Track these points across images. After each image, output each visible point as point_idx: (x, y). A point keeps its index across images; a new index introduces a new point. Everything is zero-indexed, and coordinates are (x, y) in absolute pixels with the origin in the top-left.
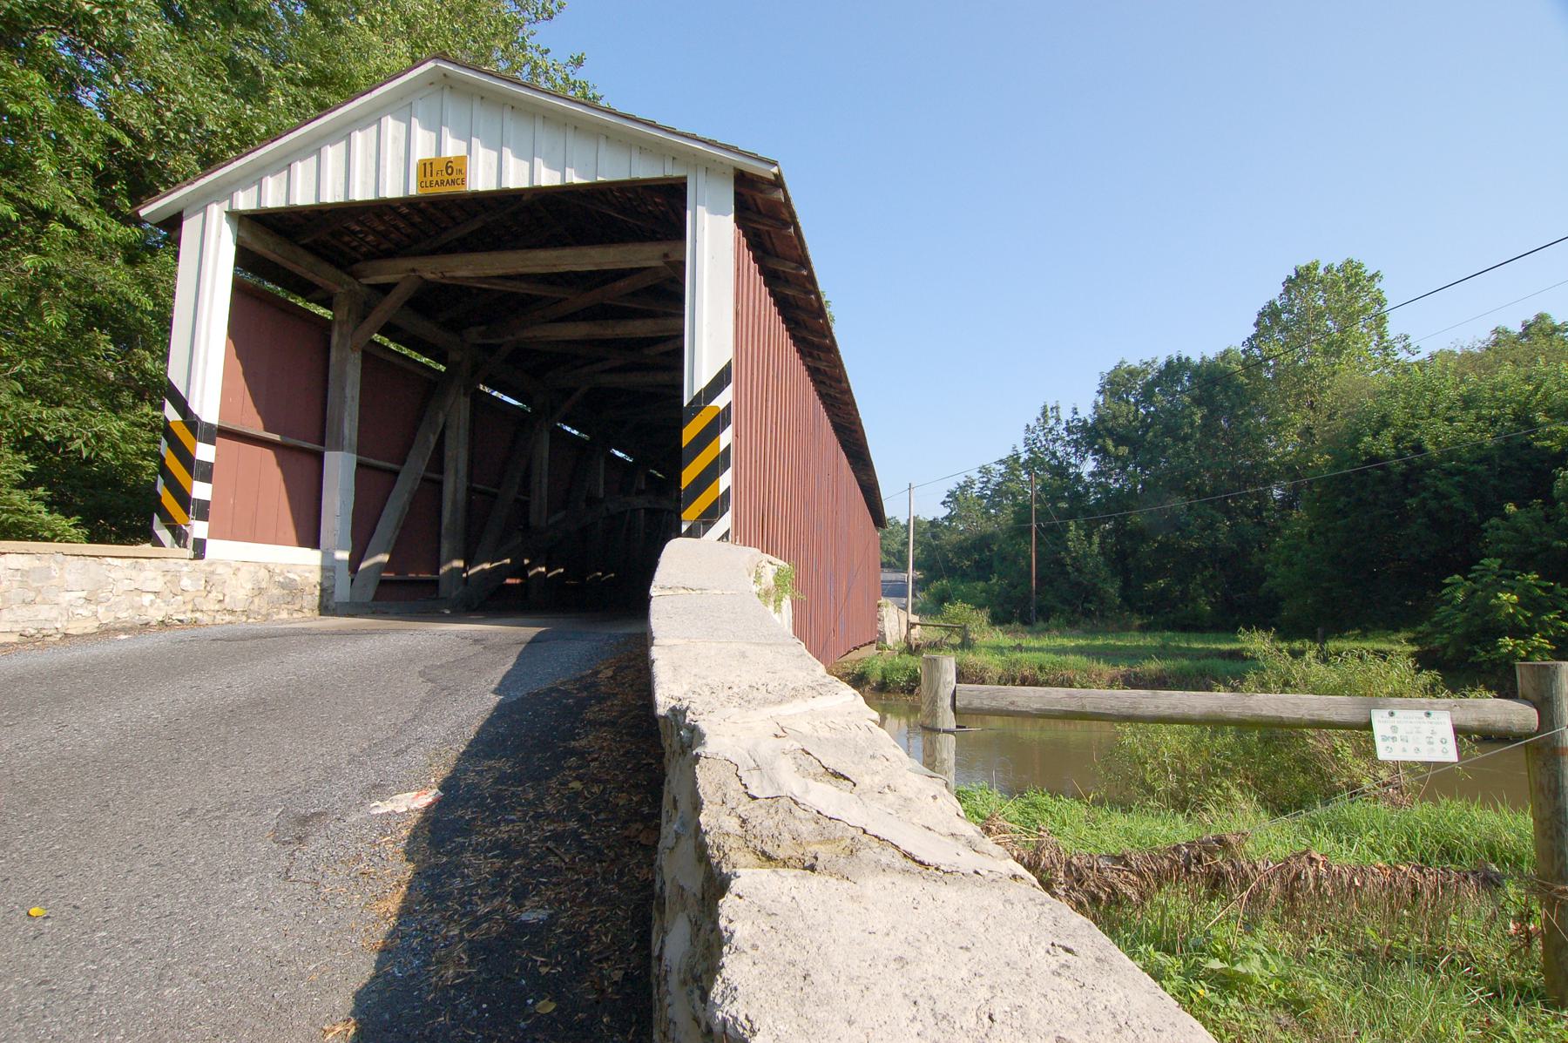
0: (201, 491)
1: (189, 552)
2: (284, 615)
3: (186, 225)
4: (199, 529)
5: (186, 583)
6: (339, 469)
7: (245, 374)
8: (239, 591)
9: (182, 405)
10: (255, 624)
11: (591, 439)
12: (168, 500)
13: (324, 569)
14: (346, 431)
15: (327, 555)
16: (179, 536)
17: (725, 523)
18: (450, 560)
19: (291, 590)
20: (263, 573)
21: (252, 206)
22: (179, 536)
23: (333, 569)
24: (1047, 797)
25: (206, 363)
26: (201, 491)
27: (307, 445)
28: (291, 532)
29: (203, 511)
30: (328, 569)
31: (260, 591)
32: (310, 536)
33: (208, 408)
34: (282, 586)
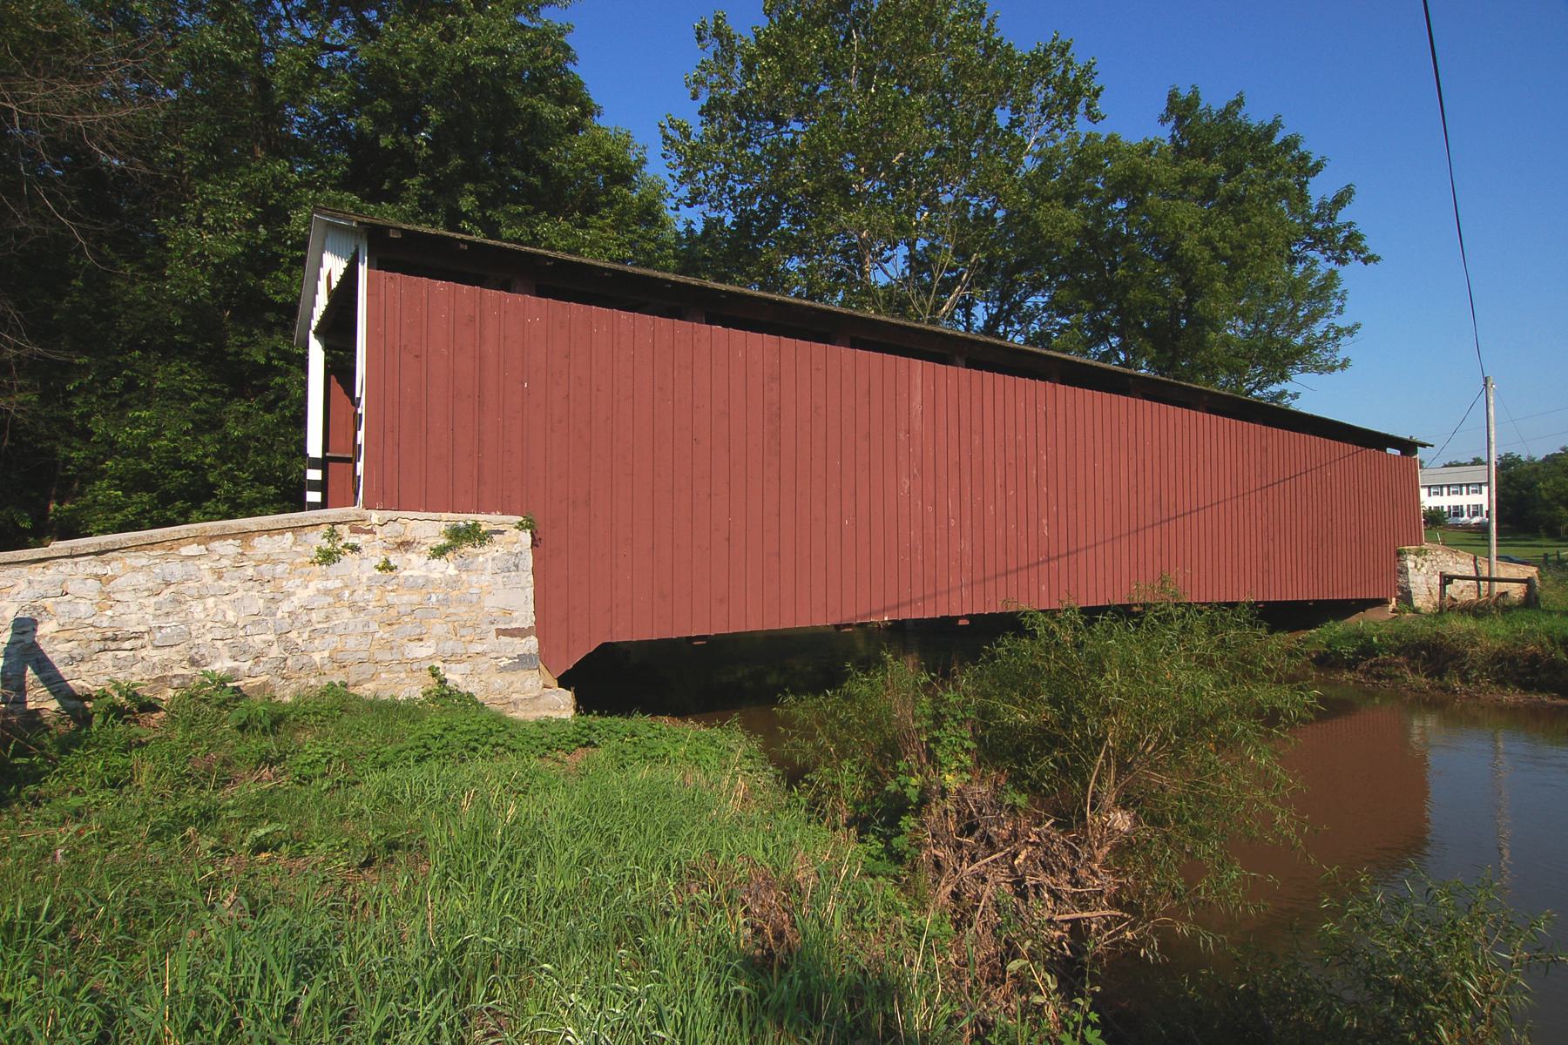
28: (376, 266)
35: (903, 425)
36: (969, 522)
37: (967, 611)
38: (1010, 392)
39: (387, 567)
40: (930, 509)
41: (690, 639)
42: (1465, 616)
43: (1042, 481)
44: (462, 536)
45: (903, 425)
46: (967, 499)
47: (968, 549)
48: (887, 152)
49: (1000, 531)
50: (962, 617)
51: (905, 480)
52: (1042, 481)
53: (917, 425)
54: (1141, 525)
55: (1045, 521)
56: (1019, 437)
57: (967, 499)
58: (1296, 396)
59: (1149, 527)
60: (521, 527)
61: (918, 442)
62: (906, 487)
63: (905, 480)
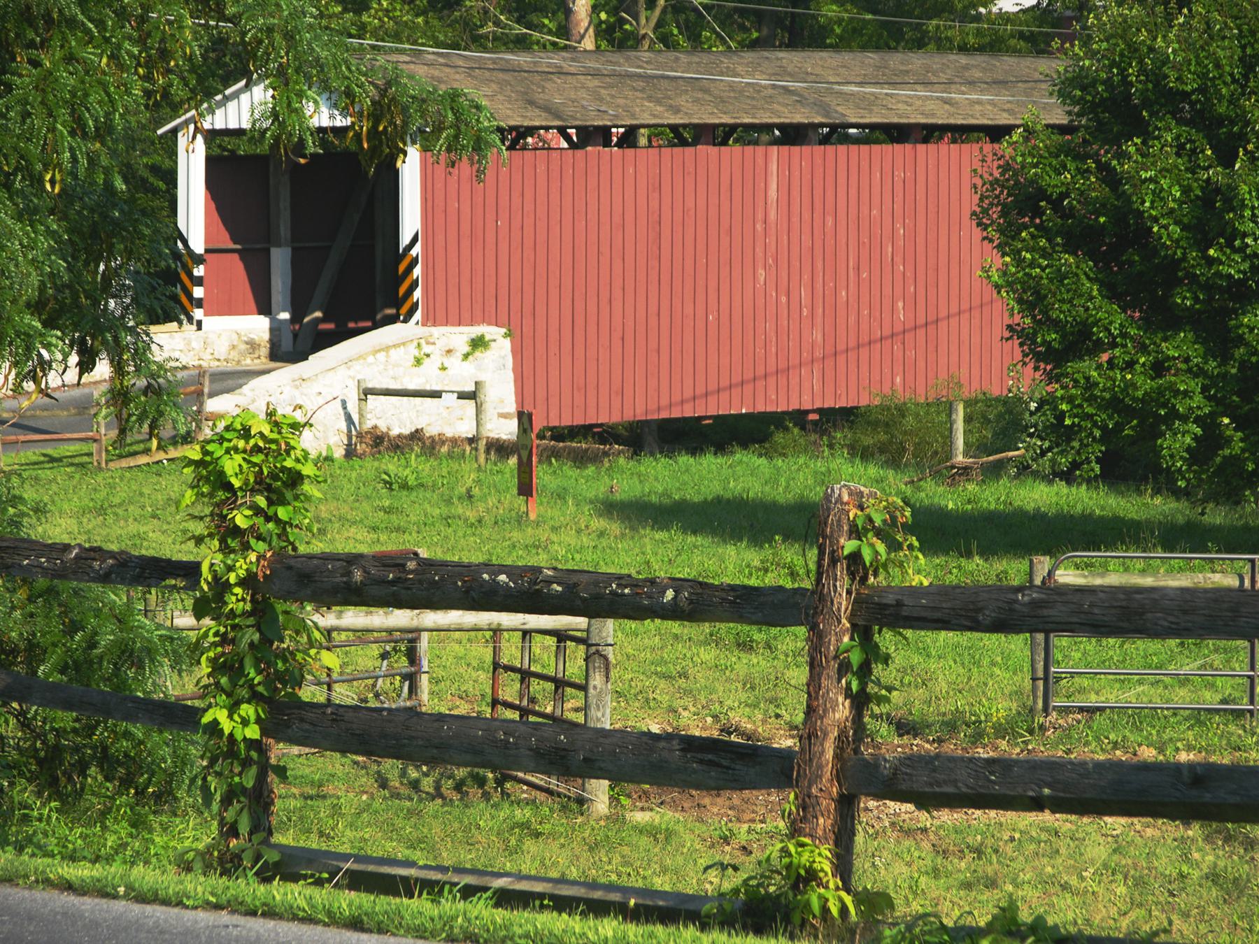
0: (198, 292)
1: (194, 327)
2: (248, 361)
3: (180, 134)
4: (198, 314)
5: (194, 344)
6: (280, 259)
7: (217, 209)
8: (222, 349)
9: (185, 242)
10: (231, 367)
11: (337, 326)
12: (184, 277)
13: (272, 330)
14: (282, 233)
15: (273, 321)
16: (190, 319)
17: (418, 315)
18: (383, 308)
19: (253, 345)
20: (235, 337)
21: (210, 127)
22: (190, 319)
23: (279, 329)
24: (977, 559)
25: (356, 924)
26: (198, 292)
27: (258, 246)
28: (252, 305)
29: (199, 303)
30: (275, 330)
31: (234, 347)
32: (264, 308)
33: (198, 246)
34: (247, 343)
35: (760, 216)
36: (821, 310)
37: (818, 405)
38: (865, 165)
39: (443, 369)
40: (784, 299)
41: (700, 418)
42: (1097, 488)
43: (898, 259)
44: (478, 343)
45: (760, 216)
46: (819, 286)
47: (820, 338)
48: (145, 411)
49: (852, 319)
50: (813, 411)
51: (761, 272)
52: (898, 259)
53: (772, 215)
54: (976, 313)
55: (900, 304)
56: (874, 212)
57: (819, 286)
58: (39, 510)
59: (897, 334)
60: (506, 335)
61: (774, 230)
62: (762, 279)
63: (761, 272)
